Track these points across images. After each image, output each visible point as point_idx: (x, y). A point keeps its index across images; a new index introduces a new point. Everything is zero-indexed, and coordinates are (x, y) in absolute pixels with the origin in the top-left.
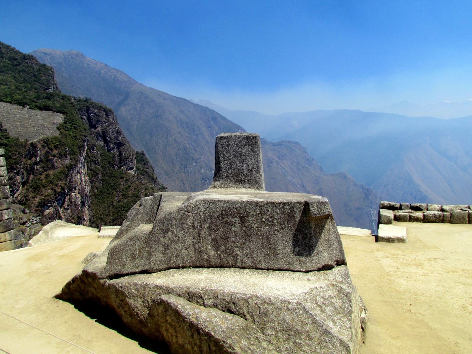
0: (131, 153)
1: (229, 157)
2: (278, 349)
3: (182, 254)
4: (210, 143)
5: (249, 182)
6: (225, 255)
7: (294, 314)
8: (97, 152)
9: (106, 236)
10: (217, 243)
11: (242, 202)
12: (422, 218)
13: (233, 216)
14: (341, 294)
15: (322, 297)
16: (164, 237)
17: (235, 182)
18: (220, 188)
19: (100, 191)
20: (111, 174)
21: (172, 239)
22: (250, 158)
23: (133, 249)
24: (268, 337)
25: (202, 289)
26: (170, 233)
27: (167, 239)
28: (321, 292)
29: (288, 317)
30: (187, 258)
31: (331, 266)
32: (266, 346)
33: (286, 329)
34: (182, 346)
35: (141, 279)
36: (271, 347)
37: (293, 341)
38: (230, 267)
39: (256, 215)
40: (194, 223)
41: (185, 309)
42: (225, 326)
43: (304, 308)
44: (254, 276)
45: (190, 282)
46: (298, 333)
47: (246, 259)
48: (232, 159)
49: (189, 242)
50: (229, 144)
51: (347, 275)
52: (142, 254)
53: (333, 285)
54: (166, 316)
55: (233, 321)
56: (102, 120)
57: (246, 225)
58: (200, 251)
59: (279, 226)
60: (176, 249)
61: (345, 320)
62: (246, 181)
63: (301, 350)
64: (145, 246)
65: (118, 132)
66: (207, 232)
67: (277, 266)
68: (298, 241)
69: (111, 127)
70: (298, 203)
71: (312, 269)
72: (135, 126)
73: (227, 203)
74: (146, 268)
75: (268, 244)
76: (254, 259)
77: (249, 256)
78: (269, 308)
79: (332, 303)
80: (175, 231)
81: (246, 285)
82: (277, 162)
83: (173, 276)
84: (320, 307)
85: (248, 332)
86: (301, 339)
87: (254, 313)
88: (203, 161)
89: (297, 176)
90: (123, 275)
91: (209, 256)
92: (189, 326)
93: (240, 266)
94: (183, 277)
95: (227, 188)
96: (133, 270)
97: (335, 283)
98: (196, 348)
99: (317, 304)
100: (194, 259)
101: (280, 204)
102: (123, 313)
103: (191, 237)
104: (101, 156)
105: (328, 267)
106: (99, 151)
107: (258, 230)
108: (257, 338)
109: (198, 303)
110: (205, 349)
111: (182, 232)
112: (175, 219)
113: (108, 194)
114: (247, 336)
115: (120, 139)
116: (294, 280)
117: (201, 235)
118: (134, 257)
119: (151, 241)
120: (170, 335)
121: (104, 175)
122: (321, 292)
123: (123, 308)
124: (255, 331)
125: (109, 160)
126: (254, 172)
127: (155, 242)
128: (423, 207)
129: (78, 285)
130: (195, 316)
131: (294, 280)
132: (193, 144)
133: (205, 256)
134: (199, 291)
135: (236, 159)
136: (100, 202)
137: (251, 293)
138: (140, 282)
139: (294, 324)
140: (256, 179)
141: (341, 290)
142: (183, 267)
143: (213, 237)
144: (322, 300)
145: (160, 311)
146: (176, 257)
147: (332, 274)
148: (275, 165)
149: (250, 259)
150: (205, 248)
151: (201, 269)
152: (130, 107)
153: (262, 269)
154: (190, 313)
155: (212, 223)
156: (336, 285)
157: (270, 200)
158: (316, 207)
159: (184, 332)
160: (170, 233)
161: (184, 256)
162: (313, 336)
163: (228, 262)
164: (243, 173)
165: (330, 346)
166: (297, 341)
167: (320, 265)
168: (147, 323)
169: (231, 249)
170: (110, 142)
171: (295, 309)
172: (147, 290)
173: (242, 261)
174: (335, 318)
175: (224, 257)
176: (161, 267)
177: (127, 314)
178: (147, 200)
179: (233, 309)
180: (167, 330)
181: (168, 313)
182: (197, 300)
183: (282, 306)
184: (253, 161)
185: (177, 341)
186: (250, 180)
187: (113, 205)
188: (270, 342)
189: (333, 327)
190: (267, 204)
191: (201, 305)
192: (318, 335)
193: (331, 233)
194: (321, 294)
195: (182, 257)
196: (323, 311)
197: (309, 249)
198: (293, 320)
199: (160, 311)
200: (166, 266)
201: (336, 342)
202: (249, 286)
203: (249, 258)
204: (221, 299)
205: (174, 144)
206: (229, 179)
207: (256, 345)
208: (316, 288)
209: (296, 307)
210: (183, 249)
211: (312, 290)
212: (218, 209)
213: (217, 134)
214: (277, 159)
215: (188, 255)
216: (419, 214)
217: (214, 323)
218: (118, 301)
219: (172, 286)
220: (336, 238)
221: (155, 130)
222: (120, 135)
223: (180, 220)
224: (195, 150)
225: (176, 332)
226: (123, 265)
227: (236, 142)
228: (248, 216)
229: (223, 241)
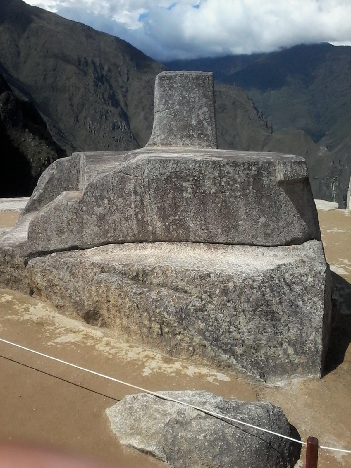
3: (121, 226)
10: (165, 213)
15: (291, 275)
16: (99, 206)
27: (102, 208)
28: (289, 269)
30: (128, 231)
39: (214, 178)
40: (135, 188)
44: (209, 252)
45: (134, 258)
48: (178, 107)
49: (131, 211)
64: (75, 217)
67: (236, 240)
74: (77, 243)
75: (227, 214)
77: (203, 228)
79: (302, 281)
80: (112, 198)
81: (201, 262)
83: (112, 252)
84: (289, 286)
94: (124, 253)
97: (305, 259)
99: (285, 282)
100: (136, 232)
103: (133, 206)
111: (120, 199)
116: (257, 255)
117: (145, 203)
118: (60, 232)
119: (82, 211)
122: (289, 269)
131: (257, 255)
133: (151, 229)
137: (208, 270)
142: (123, 242)
143: (159, 205)
146: (115, 230)
147: (303, 249)
151: (145, 244)
160: (106, 201)
163: (178, 235)
164: (191, 125)
167: (288, 239)
169: (182, 219)
174: (306, 298)
175: (174, 229)
194: (290, 272)
197: (278, 219)
202: (205, 262)
203: (204, 230)
211: (279, 267)
215: (130, 227)
228: (203, 179)
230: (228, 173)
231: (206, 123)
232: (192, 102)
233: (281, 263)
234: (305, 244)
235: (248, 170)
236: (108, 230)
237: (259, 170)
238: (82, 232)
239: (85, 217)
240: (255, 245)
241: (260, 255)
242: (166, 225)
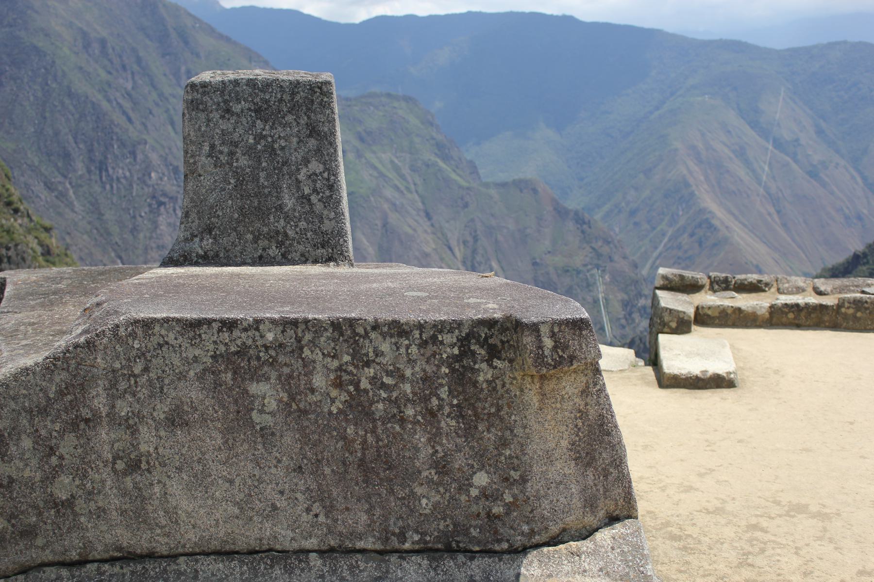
12: (767, 315)
39: (340, 368)
82: (358, 151)
89: (412, 187)
101: (421, 326)
126: (319, 207)
132: (121, 101)
157: (386, 316)
184: (315, 166)
213: (189, 74)
224: (130, 120)
230: (378, 353)
231: (319, 200)
232: (282, 148)
234: (598, 535)
235: (434, 343)
237: (464, 342)
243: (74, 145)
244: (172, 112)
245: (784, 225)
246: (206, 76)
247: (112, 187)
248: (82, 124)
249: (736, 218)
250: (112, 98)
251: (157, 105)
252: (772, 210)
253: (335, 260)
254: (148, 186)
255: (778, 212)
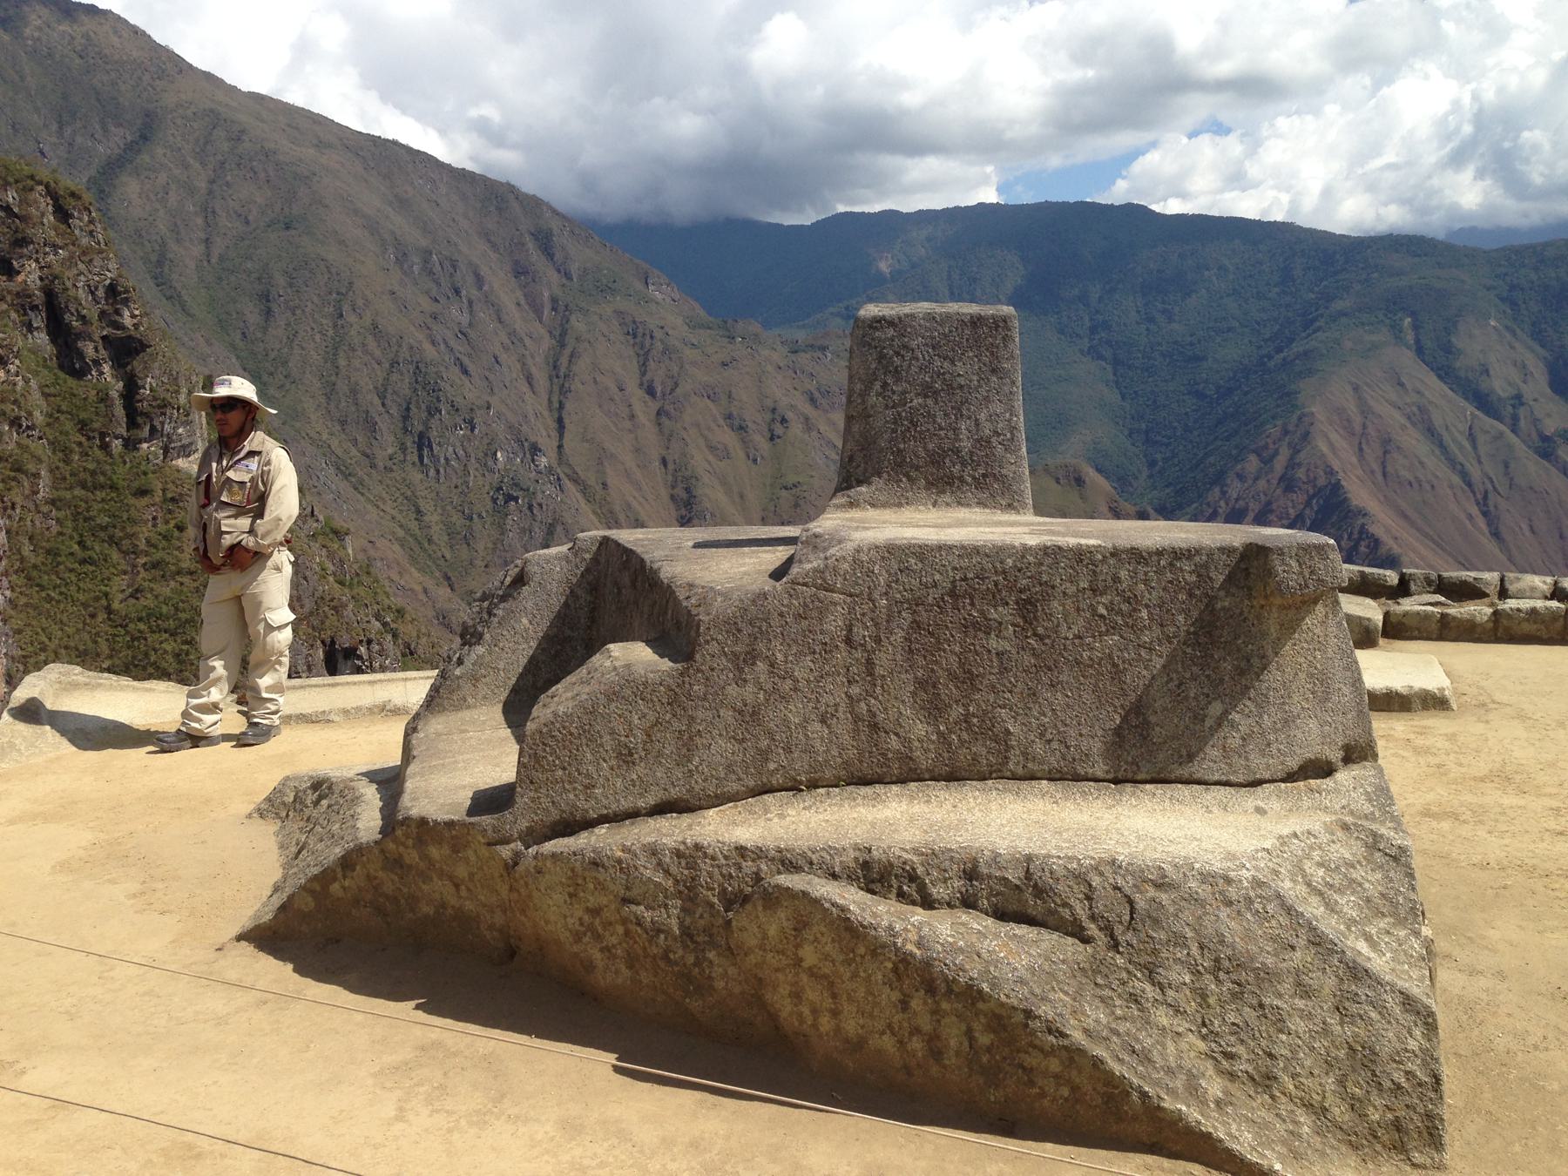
0: (182, 382)
1: (904, 392)
2: (1204, 1031)
4: (527, 341)
5: (980, 483)
6: (965, 736)
7: (1249, 916)
8: (27, 381)
9: (358, 709)
11: (1026, 549)
12: (1491, 625)
13: (994, 596)
14: (1378, 854)
15: (1320, 865)
16: (741, 681)
17: (930, 485)
18: (873, 506)
19: (48, 552)
20: (93, 473)
21: (769, 686)
22: (987, 399)
23: (621, 729)
24: (1170, 993)
25: (916, 851)
26: (761, 666)
27: (750, 688)
29: (1230, 926)
31: (1329, 763)
32: (1165, 1021)
33: (1226, 964)
34: (858, 1045)
35: (670, 831)
36: (1182, 1025)
37: (1255, 1002)
38: (983, 778)
40: (850, 629)
41: (875, 915)
42: (1021, 962)
43: (1279, 896)
46: (1266, 976)
47: (1039, 748)
49: (835, 694)
50: (905, 347)
51: (1382, 795)
52: (658, 746)
53: (1345, 827)
54: (797, 946)
55: (1044, 945)
56: (37, 234)
57: (1040, 630)
58: (876, 725)
59: (1157, 631)
60: (785, 720)
61: (1402, 933)
62: (969, 480)
63: (1281, 1031)
64: (668, 717)
65: (112, 290)
66: (899, 657)
68: (1222, 681)
69: (81, 266)
70: (1222, 549)
71: (1267, 776)
72: (192, 265)
73: (970, 556)
74: (675, 793)
76: (1068, 747)
78: (1164, 897)
80: (780, 656)
84: (1321, 894)
85: (1100, 981)
86: (1280, 996)
87: (1112, 917)
88: (499, 415)
90: (589, 824)
91: (906, 741)
92: (895, 970)
93: (1020, 771)
95: (900, 505)
96: (625, 804)
97: (1349, 819)
98: (916, 1044)
99: (1309, 885)
100: (852, 753)
101: (1160, 553)
102: (597, 956)
104: (46, 395)
105: (1323, 770)
106: (36, 374)
107: (1082, 645)
108: (1134, 998)
109: (901, 896)
110: (953, 1043)
112: (781, 615)
113: (83, 562)
114: (1099, 992)
115: (127, 321)
117: (879, 671)
118: (626, 757)
120: (806, 1011)
121: (58, 480)
122: (1311, 848)
123: (598, 937)
124: (1124, 975)
125: (83, 415)
127: (705, 699)
128: (1487, 584)
129: (369, 877)
130: (913, 936)
132: (452, 343)
133: (894, 743)
134: (905, 856)
135: (930, 402)
136: (49, 599)
138: (669, 842)
139: (1253, 948)
140: (1004, 471)
141: (1375, 842)
142: (813, 785)
144: (1321, 872)
145: (772, 931)
146: (788, 750)
147: (1337, 791)
148: (796, 429)
149: (1055, 745)
150: (892, 713)
151: (879, 788)
152: (162, 178)
153: (1096, 780)
154: (898, 927)
155: (916, 625)
156: (1355, 824)
158: (1294, 563)
159: (870, 993)
161: (817, 744)
162: (1315, 984)
164: (957, 451)
165: (1373, 1015)
166: (1267, 1001)
167: (1293, 763)
168: (710, 978)
170: (79, 336)
171: (1249, 901)
172: (705, 866)
173: (1025, 754)
176: (733, 787)
177: (614, 957)
178: (548, 562)
179: (1034, 906)
180: (797, 996)
181: (808, 934)
182: (900, 888)
183: (1204, 891)
185: (838, 1030)
186: (984, 476)
187: (109, 610)
188: (1177, 1011)
189: (1372, 955)
190: (1112, 555)
191: (914, 903)
192: (1331, 982)
193: (1330, 654)
195: (809, 750)
196: (1331, 907)
198: (1248, 936)
199: (772, 931)
200: (752, 783)
201: (1391, 1002)
203: (1049, 741)
204: (990, 877)
205: (371, 343)
206: (907, 476)
207: (1133, 1020)
208: (1295, 835)
209: (1252, 894)
210: (809, 722)
212: (937, 577)
214: (808, 409)
215: (832, 742)
216: (1479, 611)
217: (985, 955)
218: (579, 913)
219: (802, 845)
220: (1347, 668)
221: (281, 281)
222: (126, 302)
223: (800, 617)
224: (465, 372)
225: (834, 996)
226: (586, 787)
227: (933, 338)
228: (1047, 597)
229: (957, 687)
233: (1286, 831)
236: (768, 750)
238: (689, 761)
239: (700, 714)
240: (1199, 782)
241: (1215, 809)
242: (939, 733)
243: (381, 409)
244: (529, 361)
245: (1496, 535)
246: (871, 310)
247: (438, 472)
248: (395, 377)
249: (1412, 524)
250: (439, 338)
251: (506, 349)
252: (1475, 511)
253: (1014, 508)
254: (492, 471)
255: (1485, 514)
